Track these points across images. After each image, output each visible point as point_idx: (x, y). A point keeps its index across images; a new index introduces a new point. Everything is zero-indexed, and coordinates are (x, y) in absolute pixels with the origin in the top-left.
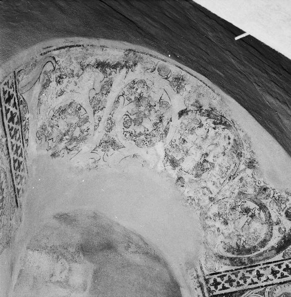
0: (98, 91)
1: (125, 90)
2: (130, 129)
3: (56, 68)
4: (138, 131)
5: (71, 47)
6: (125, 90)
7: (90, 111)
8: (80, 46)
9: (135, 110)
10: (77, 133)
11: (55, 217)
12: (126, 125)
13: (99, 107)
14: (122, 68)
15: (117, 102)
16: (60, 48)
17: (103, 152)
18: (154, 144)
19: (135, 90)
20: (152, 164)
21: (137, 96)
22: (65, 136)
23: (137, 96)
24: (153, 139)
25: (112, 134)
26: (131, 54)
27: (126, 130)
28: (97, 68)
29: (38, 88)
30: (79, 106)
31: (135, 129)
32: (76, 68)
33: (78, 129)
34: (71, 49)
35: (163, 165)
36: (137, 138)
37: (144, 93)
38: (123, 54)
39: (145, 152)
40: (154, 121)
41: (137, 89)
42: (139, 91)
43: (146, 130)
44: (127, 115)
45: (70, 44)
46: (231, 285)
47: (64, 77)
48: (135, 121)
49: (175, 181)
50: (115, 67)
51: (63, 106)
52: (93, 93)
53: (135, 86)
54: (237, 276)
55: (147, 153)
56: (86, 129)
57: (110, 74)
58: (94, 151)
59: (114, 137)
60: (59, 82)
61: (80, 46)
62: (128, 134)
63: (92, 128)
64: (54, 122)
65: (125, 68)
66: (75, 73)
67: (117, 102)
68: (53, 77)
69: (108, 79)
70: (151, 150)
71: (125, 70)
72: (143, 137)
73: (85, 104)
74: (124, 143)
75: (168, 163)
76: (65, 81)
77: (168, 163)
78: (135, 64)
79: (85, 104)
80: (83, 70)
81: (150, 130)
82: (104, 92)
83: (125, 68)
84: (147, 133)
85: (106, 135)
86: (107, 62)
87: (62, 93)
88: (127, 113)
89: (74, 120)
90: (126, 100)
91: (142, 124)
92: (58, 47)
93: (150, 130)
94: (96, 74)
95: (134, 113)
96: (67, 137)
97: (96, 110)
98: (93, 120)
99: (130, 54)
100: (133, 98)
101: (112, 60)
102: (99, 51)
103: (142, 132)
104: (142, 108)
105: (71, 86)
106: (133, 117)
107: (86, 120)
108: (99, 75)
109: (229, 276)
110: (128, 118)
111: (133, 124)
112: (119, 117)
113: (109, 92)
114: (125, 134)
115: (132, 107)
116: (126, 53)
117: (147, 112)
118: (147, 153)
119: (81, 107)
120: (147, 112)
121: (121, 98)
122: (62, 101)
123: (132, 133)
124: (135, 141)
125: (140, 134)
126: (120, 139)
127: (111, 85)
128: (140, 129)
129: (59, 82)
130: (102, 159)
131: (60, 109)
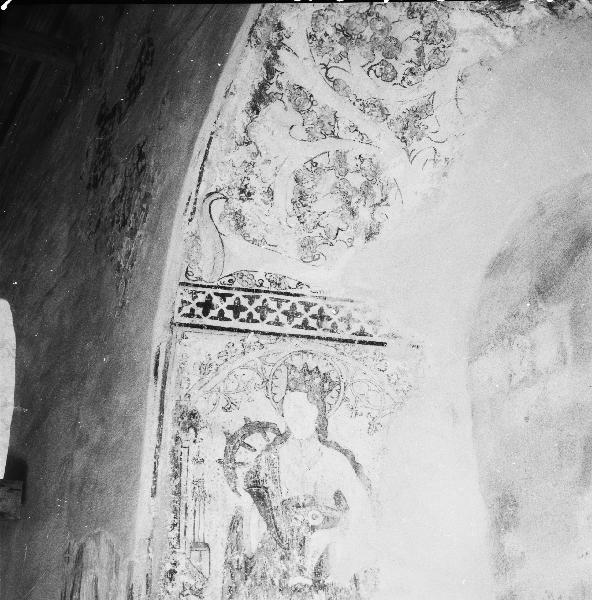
0: (297, 118)
1: (319, 60)
2: (401, 72)
3: (225, 195)
4: (412, 55)
5: (205, 159)
6: (319, 60)
7: (330, 144)
8: (211, 138)
9: (366, 49)
10: (357, 180)
11: (487, 276)
12: (389, 77)
13: (329, 123)
14: (276, 57)
15: (335, 83)
16: (200, 180)
17: (424, 139)
18: (450, 30)
19: (326, 39)
20: (493, 51)
21: (337, 38)
22: (350, 203)
23: (337, 38)
24: (440, 28)
25: (395, 111)
26: (259, 31)
27: (398, 80)
28: (258, 113)
29: (234, 241)
30: (309, 165)
31: (403, 60)
32: (244, 153)
33: (349, 176)
34: (209, 157)
35: (504, 31)
36: (426, 60)
37: (338, 21)
38: (253, 50)
39: (463, 54)
40: (404, 12)
41: (326, 35)
42: (331, 31)
43: (416, 36)
44: (370, 69)
45: (201, 158)
46: (236, 316)
47: (246, 182)
48: (388, 55)
49: (554, 17)
50: (270, 71)
51: (292, 196)
52: (300, 132)
53: (319, 35)
54: (251, 303)
55: (464, 51)
56: (358, 162)
57: (280, 86)
58: (413, 155)
59: (403, 108)
60: (249, 194)
61: (211, 138)
62: (410, 78)
63: (363, 149)
64: (309, 220)
65: (279, 52)
66: (249, 160)
67: (335, 83)
68: (236, 204)
69: (287, 94)
70: (462, 41)
71: (282, 53)
72: (428, 49)
73: (312, 150)
74: (424, 92)
75: (503, 15)
76: (254, 182)
77: (503, 15)
78: (279, 27)
79: (312, 150)
80: (248, 143)
81: (419, 28)
82: (307, 105)
83: (279, 52)
84: (422, 37)
85: (391, 123)
86: (257, 88)
87: (270, 192)
88: (366, 68)
89: (331, 178)
90: (341, 64)
91: (400, 40)
92: (197, 183)
93: (419, 28)
94: (268, 117)
95: (370, 53)
96: (354, 200)
97: (333, 132)
98: (352, 147)
99: (259, 35)
100: (339, 48)
101: (259, 76)
102: (233, 100)
103: (417, 45)
104: (368, 33)
105: (268, 171)
106: (379, 57)
107: (341, 157)
108: (273, 111)
109: (265, 301)
110: (378, 68)
111: (392, 61)
112: (367, 87)
113: (311, 96)
114: (405, 84)
115: (358, 56)
116: (254, 43)
117: (379, 25)
118: (464, 51)
119: (311, 160)
120: (379, 25)
121: (331, 73)
122: (285, 191)
123: (411, 69)
124: (430, 69)
125: (420, 52)
126: (412, 97)
127: (301, 88)
128: (410, 51)
129: (249, 194)
130: (437, 146)
131: (294, 203)
